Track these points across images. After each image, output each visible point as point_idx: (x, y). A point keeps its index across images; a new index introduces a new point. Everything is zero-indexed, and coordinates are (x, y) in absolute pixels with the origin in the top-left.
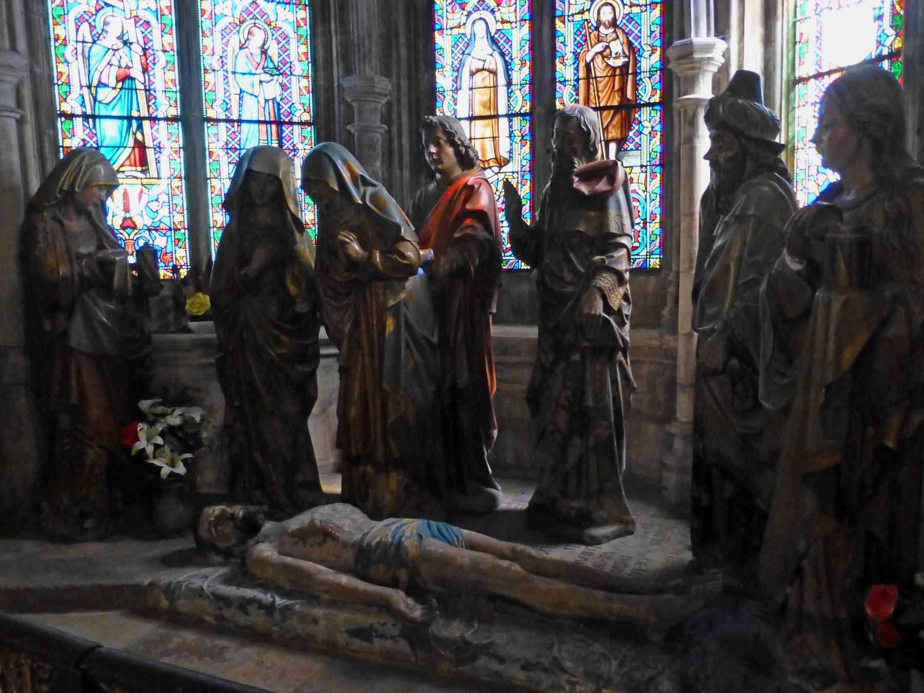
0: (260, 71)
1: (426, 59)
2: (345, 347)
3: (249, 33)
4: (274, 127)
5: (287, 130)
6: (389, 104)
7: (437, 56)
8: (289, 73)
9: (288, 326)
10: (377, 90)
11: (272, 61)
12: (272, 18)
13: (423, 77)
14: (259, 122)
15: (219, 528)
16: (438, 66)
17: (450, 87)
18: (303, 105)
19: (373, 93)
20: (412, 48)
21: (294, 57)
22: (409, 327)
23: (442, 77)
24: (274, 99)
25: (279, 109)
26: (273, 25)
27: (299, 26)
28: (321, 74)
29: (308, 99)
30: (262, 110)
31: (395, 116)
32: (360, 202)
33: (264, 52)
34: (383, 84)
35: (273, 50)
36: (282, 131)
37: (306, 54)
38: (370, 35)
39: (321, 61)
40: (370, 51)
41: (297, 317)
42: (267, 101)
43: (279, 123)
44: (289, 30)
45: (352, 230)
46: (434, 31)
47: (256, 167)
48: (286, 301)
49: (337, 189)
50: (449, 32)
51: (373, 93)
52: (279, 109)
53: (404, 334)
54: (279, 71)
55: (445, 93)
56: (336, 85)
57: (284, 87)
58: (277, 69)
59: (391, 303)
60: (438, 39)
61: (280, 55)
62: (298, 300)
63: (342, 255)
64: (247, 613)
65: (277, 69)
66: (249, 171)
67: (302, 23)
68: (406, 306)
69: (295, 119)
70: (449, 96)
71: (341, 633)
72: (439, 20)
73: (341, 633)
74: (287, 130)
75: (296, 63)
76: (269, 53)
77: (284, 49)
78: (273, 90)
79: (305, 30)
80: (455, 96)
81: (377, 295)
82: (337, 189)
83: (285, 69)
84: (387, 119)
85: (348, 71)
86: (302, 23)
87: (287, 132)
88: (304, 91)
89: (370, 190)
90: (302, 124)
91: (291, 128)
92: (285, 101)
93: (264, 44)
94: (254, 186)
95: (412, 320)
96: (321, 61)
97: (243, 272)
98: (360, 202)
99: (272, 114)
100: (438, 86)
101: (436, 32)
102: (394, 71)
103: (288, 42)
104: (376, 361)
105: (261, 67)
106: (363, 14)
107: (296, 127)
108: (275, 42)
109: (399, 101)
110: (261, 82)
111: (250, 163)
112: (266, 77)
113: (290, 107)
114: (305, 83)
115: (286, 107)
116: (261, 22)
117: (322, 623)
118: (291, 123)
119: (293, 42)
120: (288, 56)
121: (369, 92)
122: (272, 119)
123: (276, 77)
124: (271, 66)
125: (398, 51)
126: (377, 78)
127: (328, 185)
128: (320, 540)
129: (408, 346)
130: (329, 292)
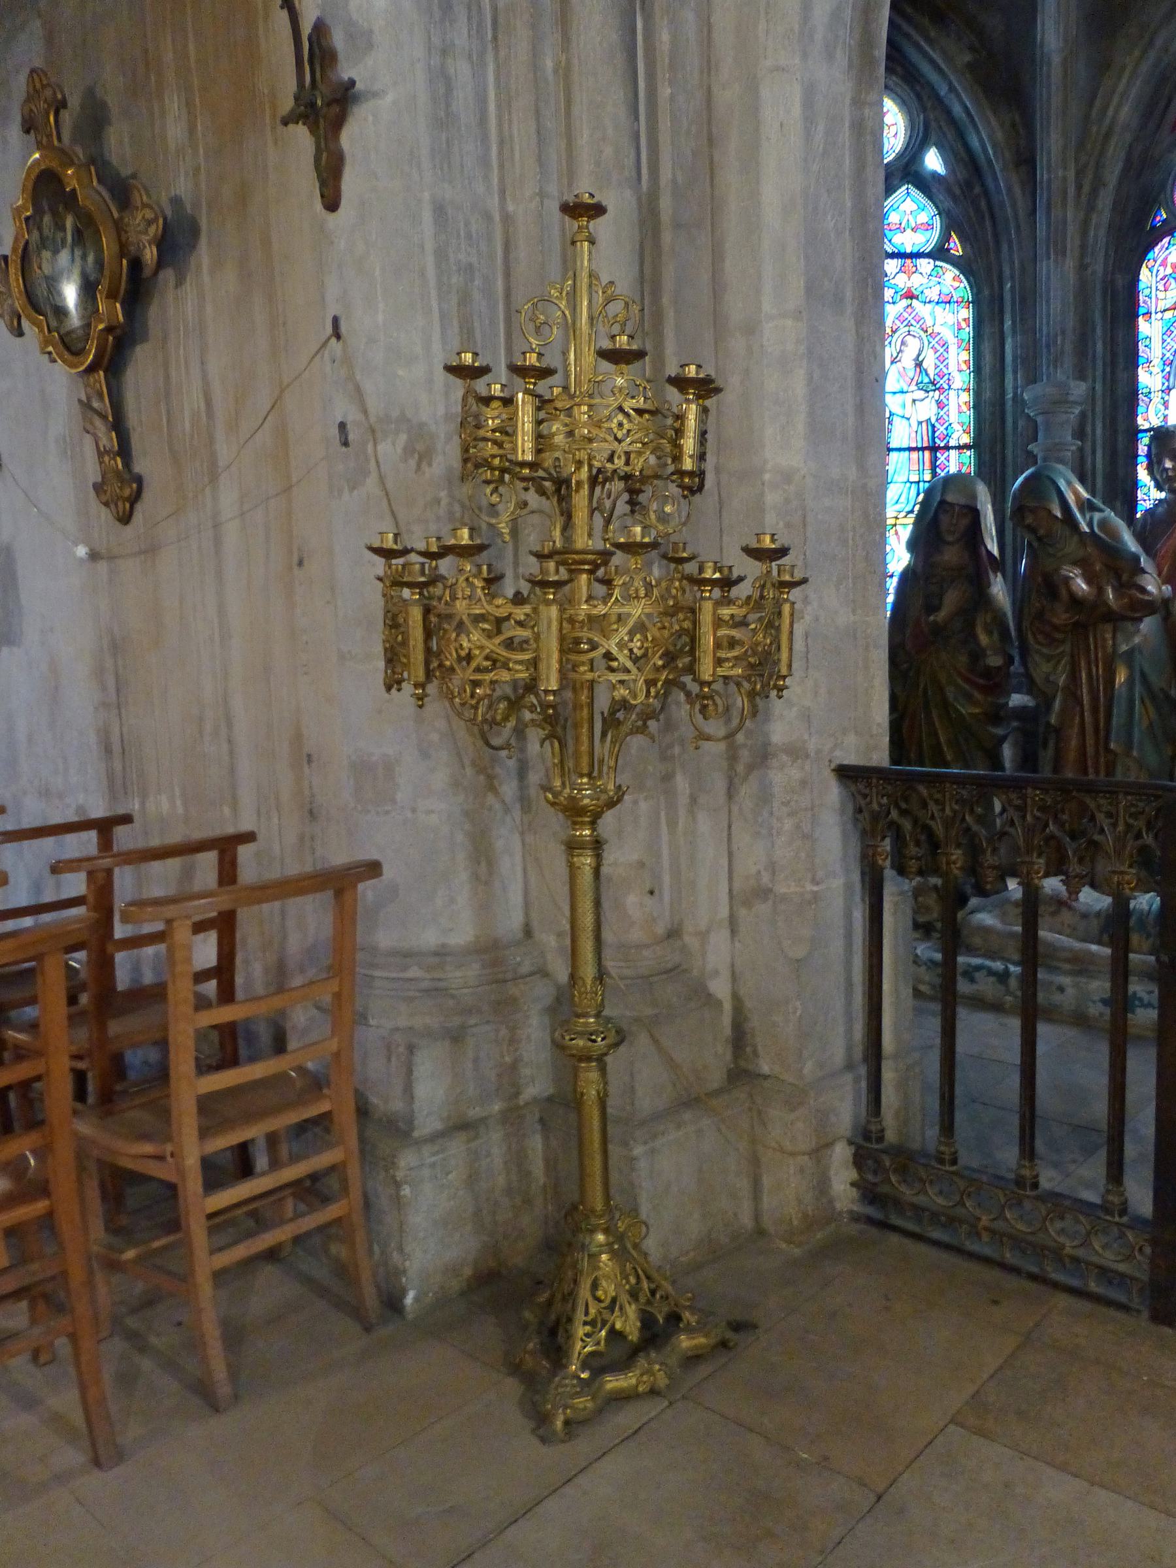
0: (913, 387)
1: (1125, 354)
2: (1000, 731)
3: (903, 343)
4: (927, 453)
5: (941, 457)
6: (1083, 415)
7: (1141, 347)
8: (946, 387)
9: (981, 681)
10: (1071, 398)
11: (927, 375)
12: (929, 323)
13: (1122, 375)
14: (910, 449)
15: (920, 899)
16: (1141, 361)
17: (1159, 387)
18: (962, 424)
19: (1067, 402)
20: (1111, 342)
21: (953, 368)
22: (1143, 675)
23: (1147, 374)
24: (928, 421)
25: (934, 432)
26: (930, 331)
27: (960, 329)
28: (987, 385)
29: (968, 416)
30: (914, 435)
31: (1089, 429)
32: (1087, 530)
33: (919, 365)
34: (1079, 389)
35: (929, 363)
36: (936, 459)
37: (967, 362)
38: (1063, 333)
39: (987, 370)
40: (1062, 352)
41: (988, 673)
42: (920, 423)
43: (934, 449)
44: (948, 335)
45: (1075, 563)
46: (1138, 316)
47: (950, 498)
48: (976, 655)
49: (1059, 515)
50: (1159, 315)
51: (1067, 402)
52: (934, 432)
53: (1138, 689)
54: (935, 386)
55: (1152, 395)
56: (1010, 396)
57: (940, 405)
58: (933, 383)
59: (1124, 648)
60: (1143, 327)
61: (937, 367)
62: (988, 652)
63: (1064, 592)
64: (972, 980)
65: (933, 383)
66: (942, 502)
67: (964, 325)
68: (1141, 652)
69: (952, 443)
70: (1157, 398)
71: (1094, 1002)
72: (1144, 302)
73: (1094, 1002)
74: (941, 457)
75: (955, 374)
76: (925, 365)
77: (942, 359)
78: (927, 409)
79: (968, 332)
80: (1166, 398)
81: (1104, 640)
82: (1059, 515)
83: (942, 382)
84: (1080, 434)
85: (1032, 379)
86: (964, 325)
87: (942, 459)
88: (964, 408)
89: (1097, 516)
90: (960, 448)
91: (946, 454)
92: (942, 421)
93: (919, 355)
94: (945, 519)
95: (1147, 669)
96: (987, 370)
97: (932, 618)
98: (1087, 530)
99: (925, 438)
100: (1140, 386)
101: (1140, 319)
102: (1089, 373)
103: (947, 350)
104: (1102, 715)
105: (914, 383)
106: (1056, 306)
107: (952, 452)
108: (931, 352)
109: (1093, 410)
110: (914, 401)
111: (942, 495)
112: (922, 394)
113: (946, 429)
114: (965, 397)
115: (942, 429)
116: (916, 330)
117: (1070, 991)
118: (947, 448)
119: (953, 349)
120: (947, 366)
121: (1062, 401)
122: (925, 445)
123: (931, 394)
124: (926, 380)
125: (1095, 344)
126: (1072, 383)
127: (1050, 512)
128: (1052, 909)
129: (1142, 701)
130: (1040, 637)
